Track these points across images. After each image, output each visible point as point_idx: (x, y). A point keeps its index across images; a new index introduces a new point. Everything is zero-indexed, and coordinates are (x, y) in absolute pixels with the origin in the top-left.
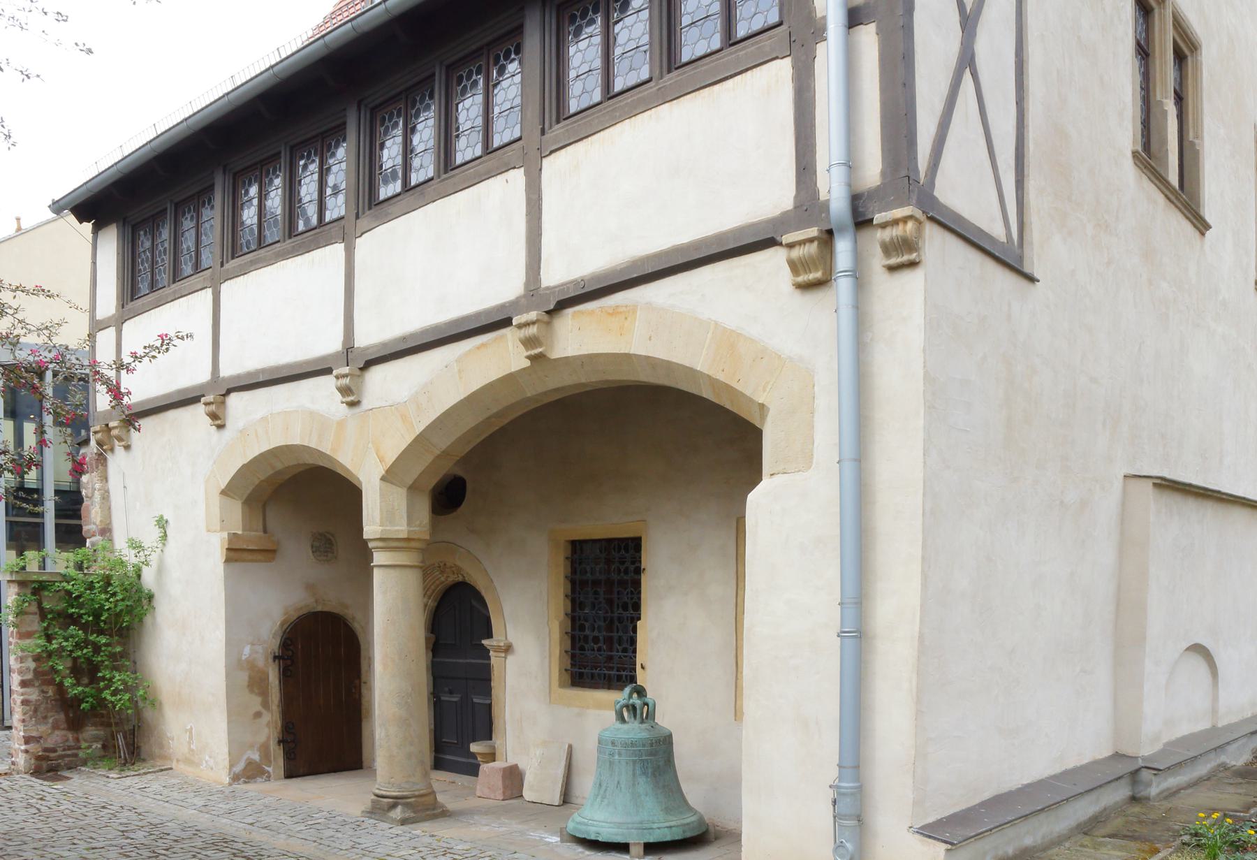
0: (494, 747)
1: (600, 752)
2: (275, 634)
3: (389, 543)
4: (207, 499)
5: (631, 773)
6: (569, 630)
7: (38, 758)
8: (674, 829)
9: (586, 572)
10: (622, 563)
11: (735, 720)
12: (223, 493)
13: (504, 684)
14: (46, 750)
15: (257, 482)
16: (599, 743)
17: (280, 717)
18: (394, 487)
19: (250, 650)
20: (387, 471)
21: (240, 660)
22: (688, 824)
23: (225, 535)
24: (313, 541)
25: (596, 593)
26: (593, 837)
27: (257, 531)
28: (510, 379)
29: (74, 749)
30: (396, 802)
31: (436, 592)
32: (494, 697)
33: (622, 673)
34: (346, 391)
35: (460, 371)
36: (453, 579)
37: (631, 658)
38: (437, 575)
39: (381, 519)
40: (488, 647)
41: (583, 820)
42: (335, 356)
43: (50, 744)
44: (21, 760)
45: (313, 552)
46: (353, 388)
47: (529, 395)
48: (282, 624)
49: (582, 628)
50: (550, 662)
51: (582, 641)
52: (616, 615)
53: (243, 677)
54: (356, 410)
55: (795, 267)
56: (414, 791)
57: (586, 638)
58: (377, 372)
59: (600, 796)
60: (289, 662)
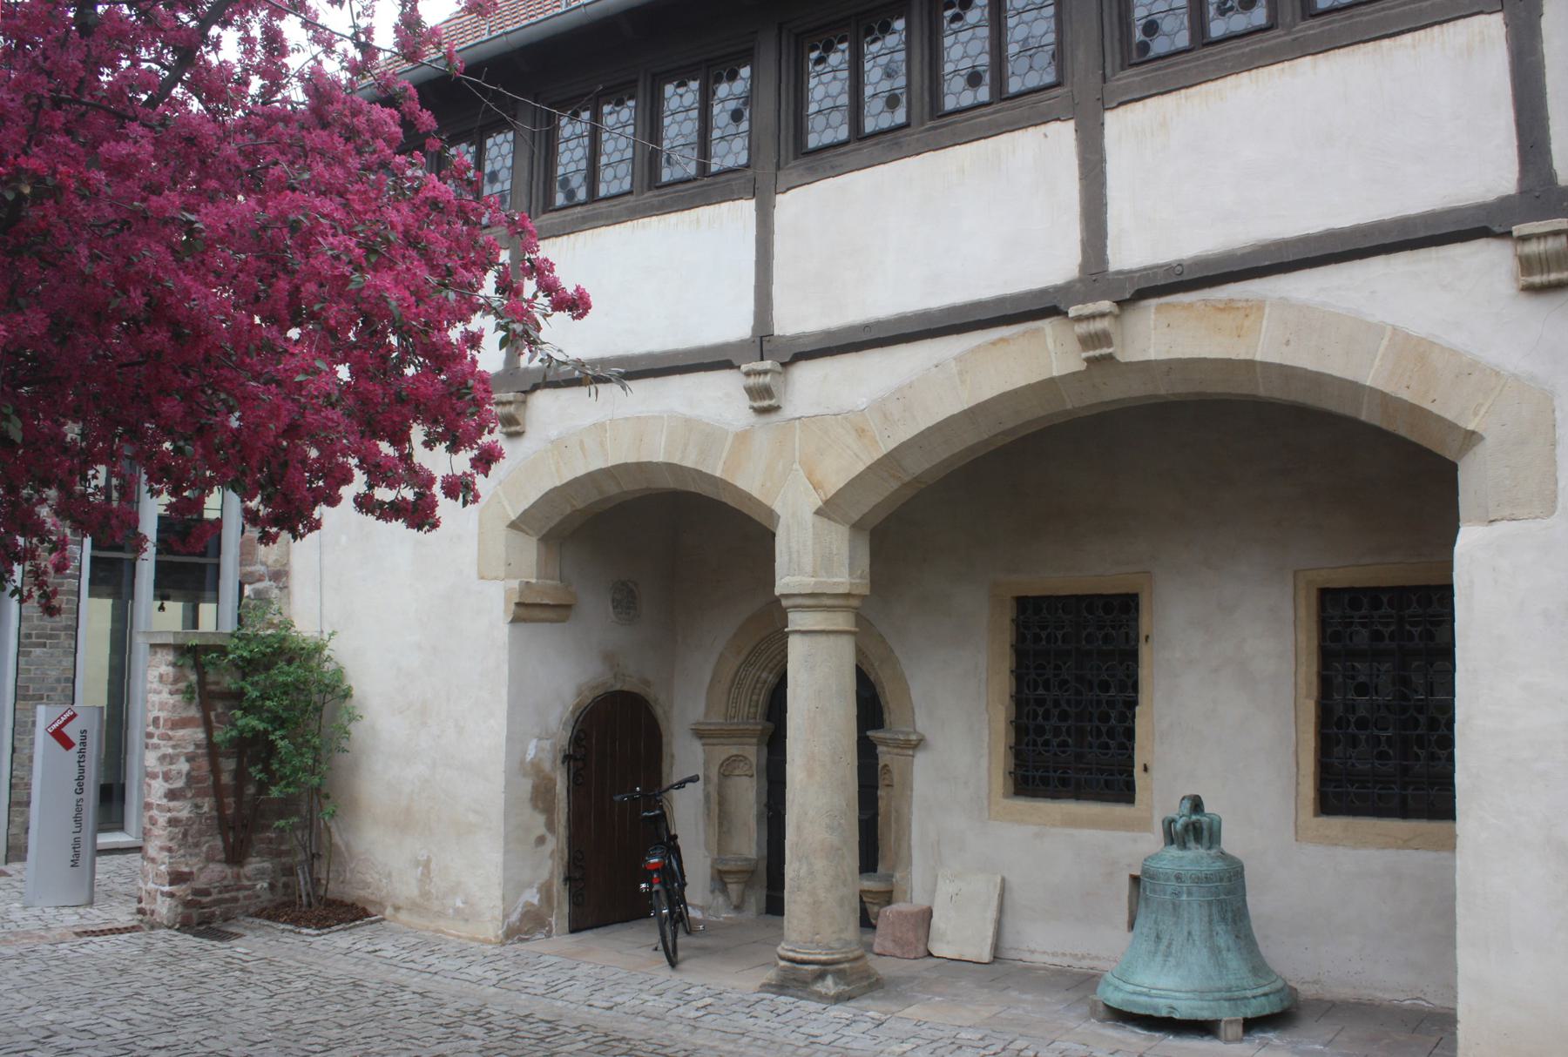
2: (565, 724)
3: (816, 600)
4: (481, 534)
5: (1206, 919)
7: (187, 904)
8: (1271, 997)
9: (1041, 640)
11: (1297, 840)
12: (513, 525)
14: (197, 892)
15: (568, 510)
18: (832, 523)
19: (536, 747)
20: (826, 503)
21: (522, 762)
26: (1164, 1013)
27: (553, 579)
28: (1050, 384)
29: (232, 890)
34: (756, 393)
35: (960, 373)
42: (740, 346)
43: (200, 883)
44: (163, 908)
45: (614, 608)
46: (773, 389)
47: (1069, 407)
48: (573, 712)
53: (527, 785)
54: (773, 418)
55: (1527, 265)
56: (846, 952)
58: (807, 375)
60: (580, 764)
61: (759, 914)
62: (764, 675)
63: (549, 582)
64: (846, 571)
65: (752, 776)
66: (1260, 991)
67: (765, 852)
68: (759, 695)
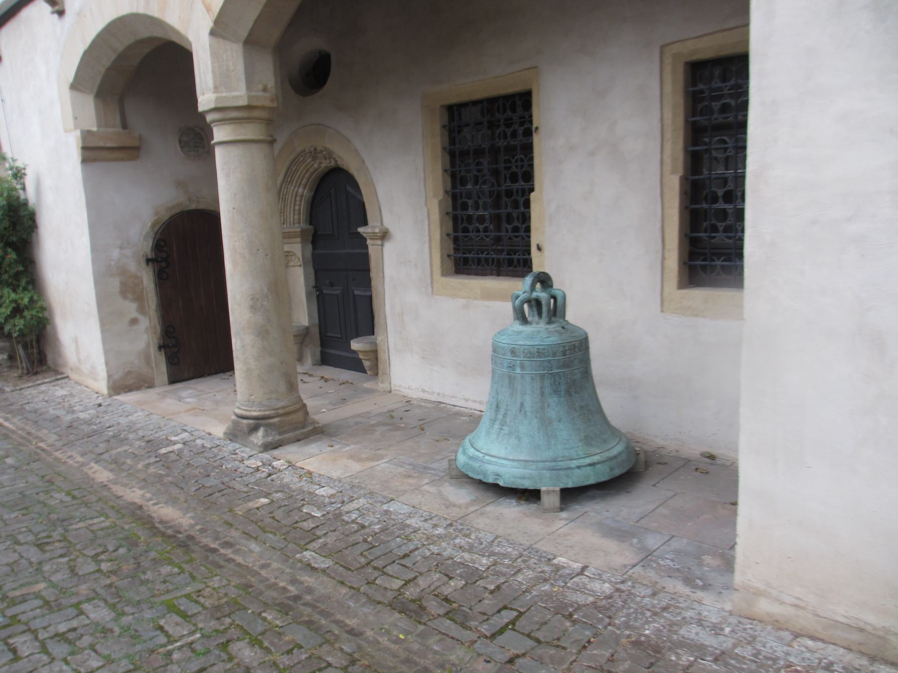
0: (376, 343)
1: (496, 362)
6: (450, 210)
10: (508, 125)
13: (382, 275)
15: (103, 70)
16: (494, 351)
17: (159, 322)
20: (217, 22)
22: (615, 457)
23: (78, 133)
24: (181, 136)
25: (478, 164)
26: (491, 480)
30: (257, 423)
31: (311, 180)
32: (373, 289)
33: (513, 256)
36: (326, 164)
37: (523, 238)
38: (309, 163)
39: (215, 83)
40: (365, 235)
41: (477, 453)
45: (181, 148)
48: (153, 225)
49: (464, 207)
50: (430, 248)
51: (465, 222)
52: (503, 188)
57: (469, 219)
59: (498, 423)
60: (164, 264)
61: (314, 365)
62: (300, 190)
63: (110, 130)
64: (243, 86)
65: (301, 266)
66: (588, 461)
67: (317, 321)
68: (300, 205)
